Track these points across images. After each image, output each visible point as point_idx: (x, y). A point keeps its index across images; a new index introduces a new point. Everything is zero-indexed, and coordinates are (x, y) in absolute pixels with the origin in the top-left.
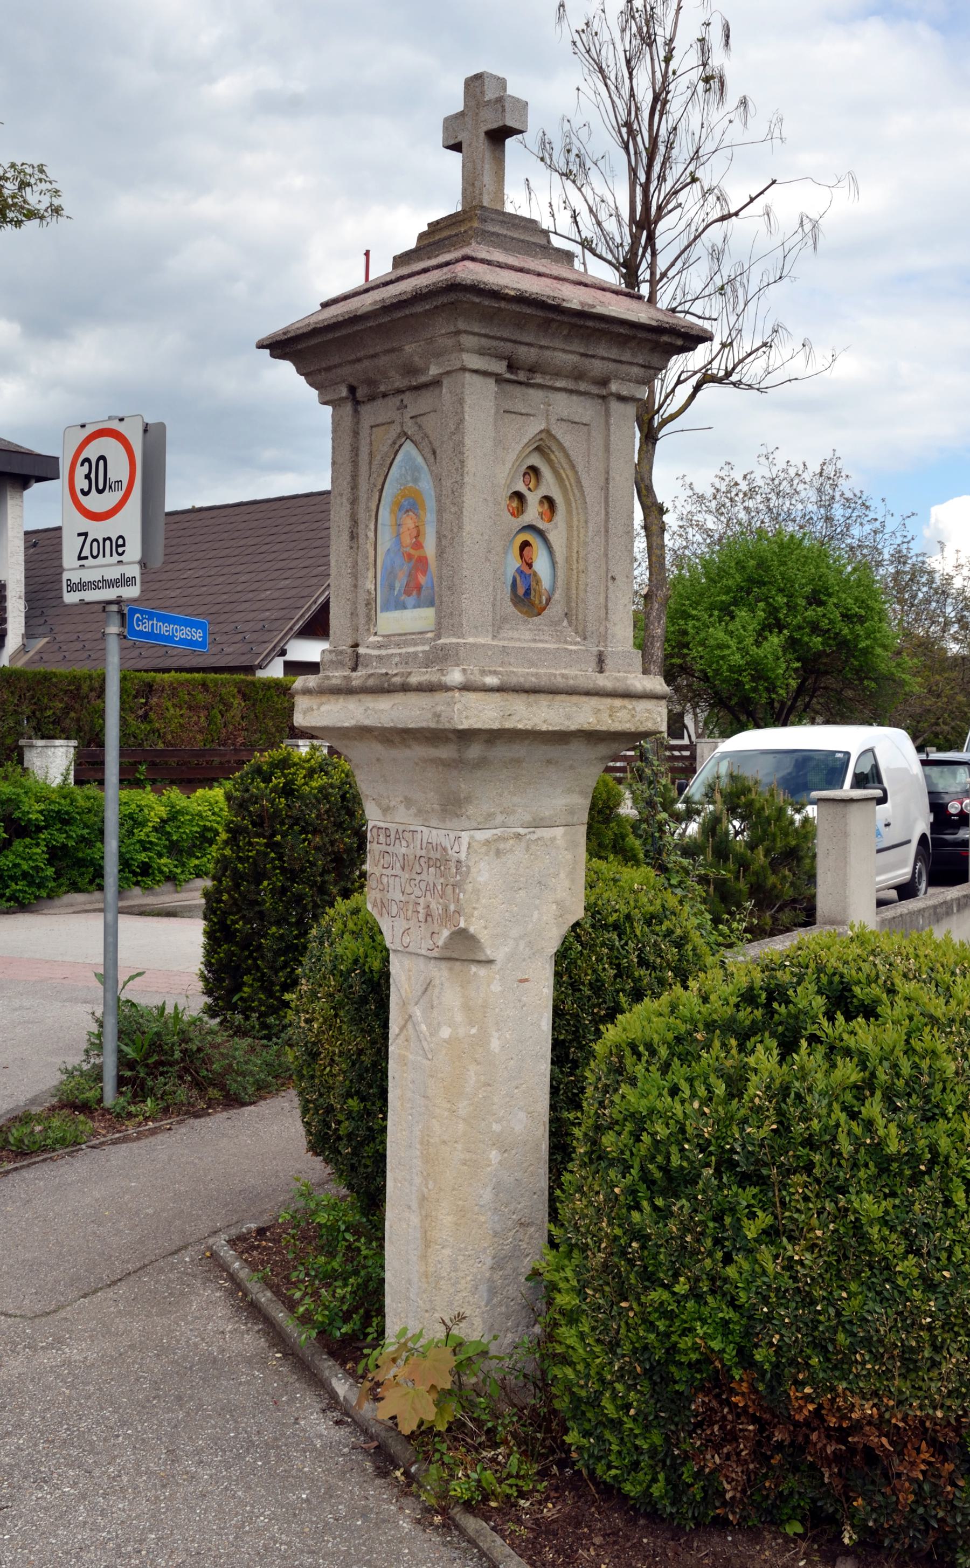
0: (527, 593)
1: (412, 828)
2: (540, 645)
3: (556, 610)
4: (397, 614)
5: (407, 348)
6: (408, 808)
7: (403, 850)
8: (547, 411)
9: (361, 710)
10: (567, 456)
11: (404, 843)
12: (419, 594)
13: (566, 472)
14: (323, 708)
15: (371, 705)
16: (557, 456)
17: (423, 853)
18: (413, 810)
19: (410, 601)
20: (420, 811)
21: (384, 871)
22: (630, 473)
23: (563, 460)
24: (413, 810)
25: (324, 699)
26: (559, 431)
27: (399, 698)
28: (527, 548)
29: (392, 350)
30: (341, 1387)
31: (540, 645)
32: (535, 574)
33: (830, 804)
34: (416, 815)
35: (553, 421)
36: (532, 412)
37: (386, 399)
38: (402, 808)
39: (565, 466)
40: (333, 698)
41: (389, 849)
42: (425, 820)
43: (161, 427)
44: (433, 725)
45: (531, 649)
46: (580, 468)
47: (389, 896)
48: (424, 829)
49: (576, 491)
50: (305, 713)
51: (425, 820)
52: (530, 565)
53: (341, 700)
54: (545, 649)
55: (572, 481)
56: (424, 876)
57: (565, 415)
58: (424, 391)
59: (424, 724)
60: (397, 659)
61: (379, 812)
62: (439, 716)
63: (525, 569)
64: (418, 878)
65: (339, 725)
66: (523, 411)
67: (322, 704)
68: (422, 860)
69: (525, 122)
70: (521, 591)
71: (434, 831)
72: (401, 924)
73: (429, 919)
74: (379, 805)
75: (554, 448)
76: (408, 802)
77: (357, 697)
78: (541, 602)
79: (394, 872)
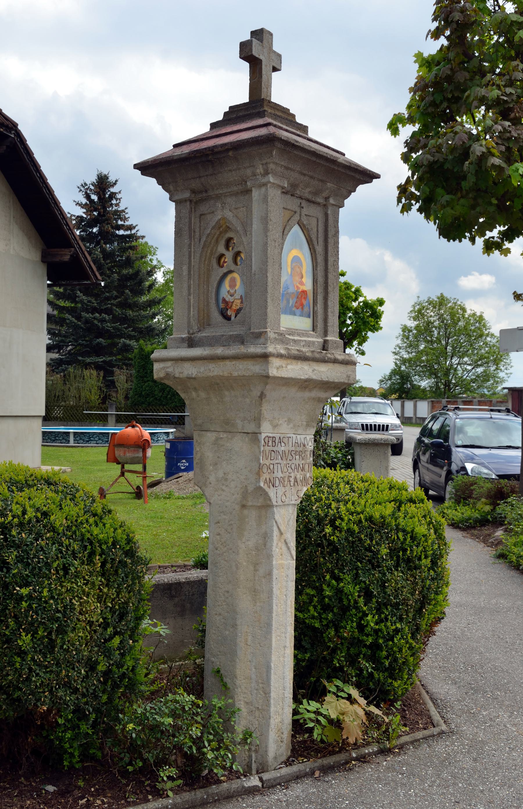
1: (288, 435)
4: (291, 317)
5: (328, 184)
6: (288, 425)
7: (283, 448)
9: (311, 370)
11: (283, 444)
12: (302, 309)
14: (289, 367)
15: (316, 368)
17: (293, 449)
18: (291, 425)
19: (298, 312)
20: (294, 426)
21: (272, 462)
24: (291, 425)
25: (289, 361)
27: (331, 366)
29: (322, 181)
30: (254, 781)
33: (10, 419)
34: (291, 428)
37: (292, 198)
38: (285, 425)
40: (294, 362)
41: (275, 449)
42: (296, 430)
43: (506, 255)
44: (346, 381)
47: (275, 475)
48: (294, 436)
50: (278, 368)
51: (296, 430)
53: (299, 363)
56: (294, 461)
58: (312, 205)
59: (342, 381)
60: (304, 343)
61: (270, 427)
62: (349, 377)
64: (290, 463)
65: (299, 377)
67: (288, 364)
68: (293, 452)
69: (281, 66)
71: (299, 437)
72: (281, 490)
73: (296, 484)
74: (271, 424)
76: (289, 421)
77: (307, 363)
79: (277, 461)
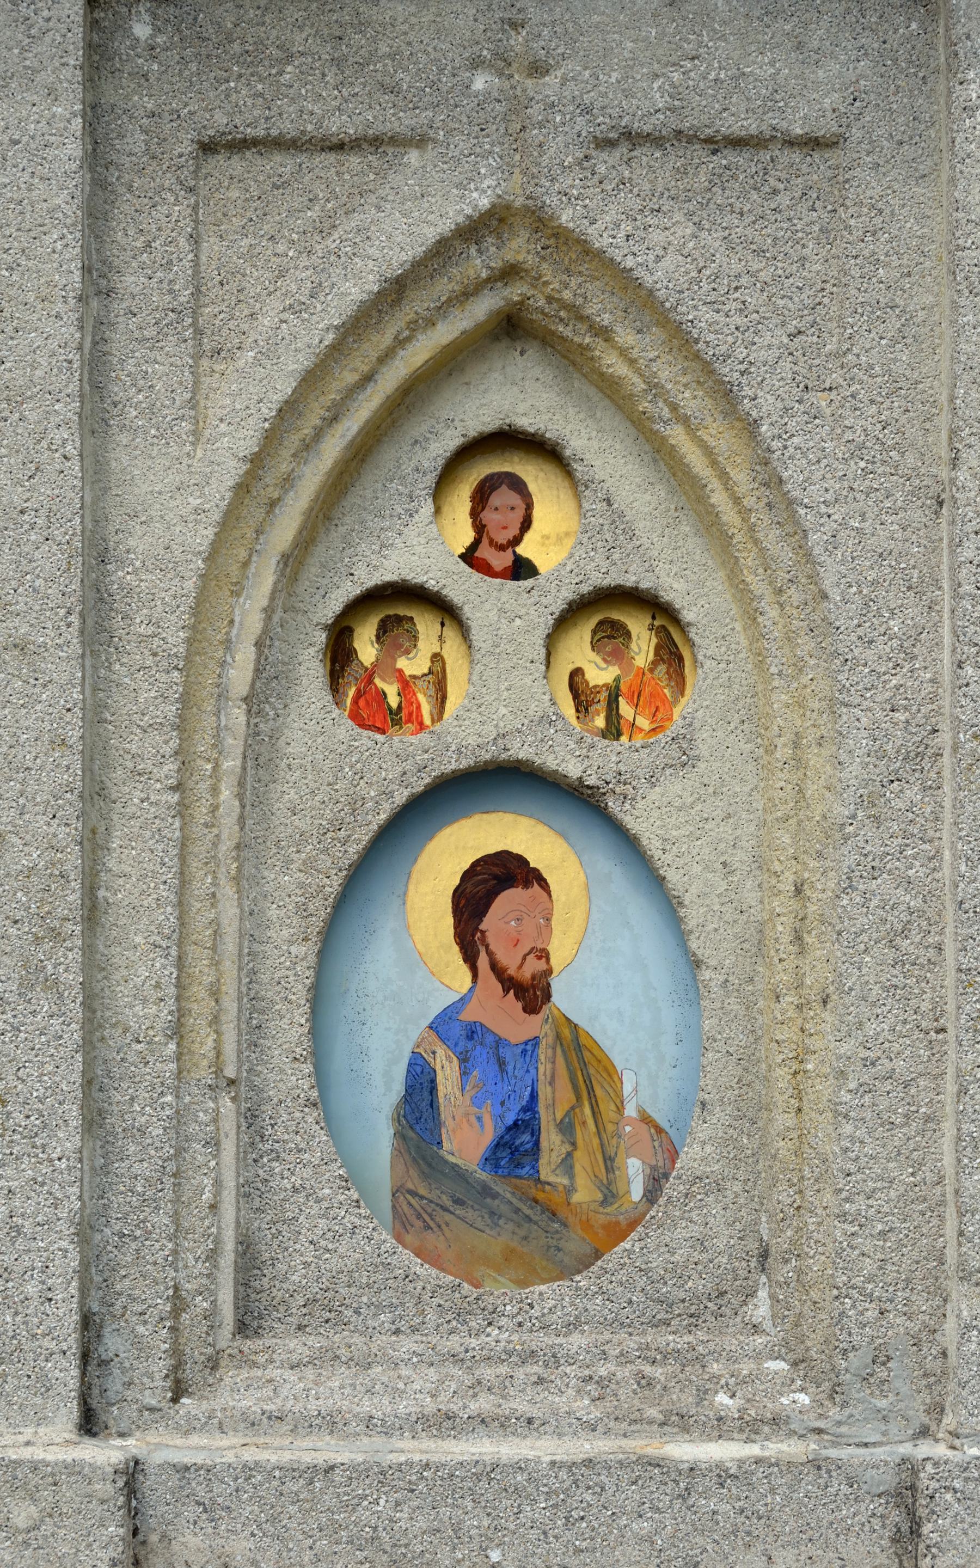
0: (515, 1146)
2: (484, 1448)
3: (682, 1241)
8: (518, 105)
10: (681, 339)
13: (703, 440)
16: (631, 351)
22: (527, 422)
23: (667, 372)
26: (602, 215)
28: (507, 906)
31: (484, 1448)
32: (577, 1048)
35: (559, 147)
36: (400, 122)
39: (692, 401)
45: (383, 1476)
46: (765, 403)
49: (771, 537)
52: (532, 993)
54: (488, 1471)
55: (741, 477)
57: (649, 103)
63: (507, 1020)
66: (336, 125)
70: (466, 1138)
75: (601, 308)
78: (610, 1195)
